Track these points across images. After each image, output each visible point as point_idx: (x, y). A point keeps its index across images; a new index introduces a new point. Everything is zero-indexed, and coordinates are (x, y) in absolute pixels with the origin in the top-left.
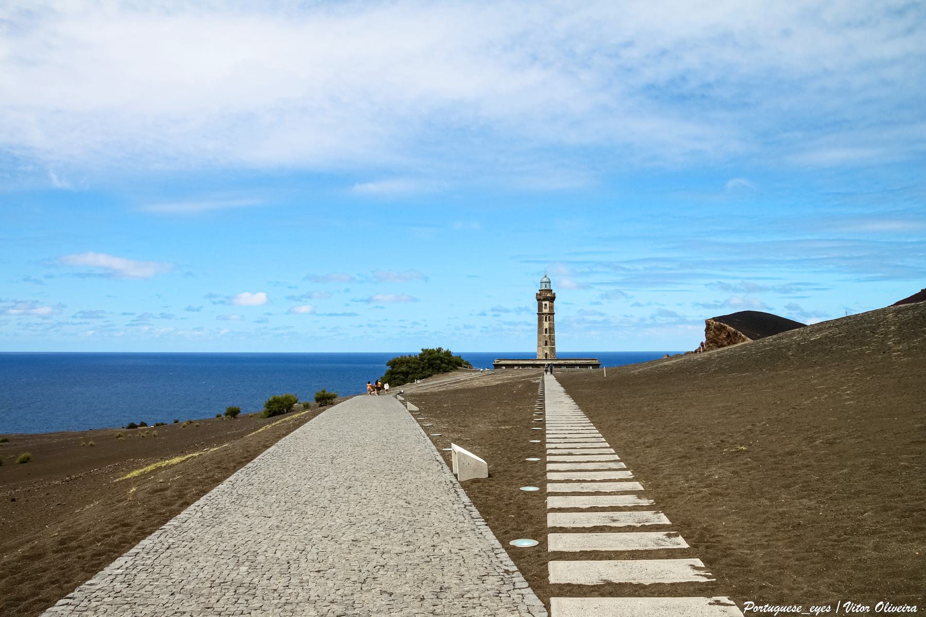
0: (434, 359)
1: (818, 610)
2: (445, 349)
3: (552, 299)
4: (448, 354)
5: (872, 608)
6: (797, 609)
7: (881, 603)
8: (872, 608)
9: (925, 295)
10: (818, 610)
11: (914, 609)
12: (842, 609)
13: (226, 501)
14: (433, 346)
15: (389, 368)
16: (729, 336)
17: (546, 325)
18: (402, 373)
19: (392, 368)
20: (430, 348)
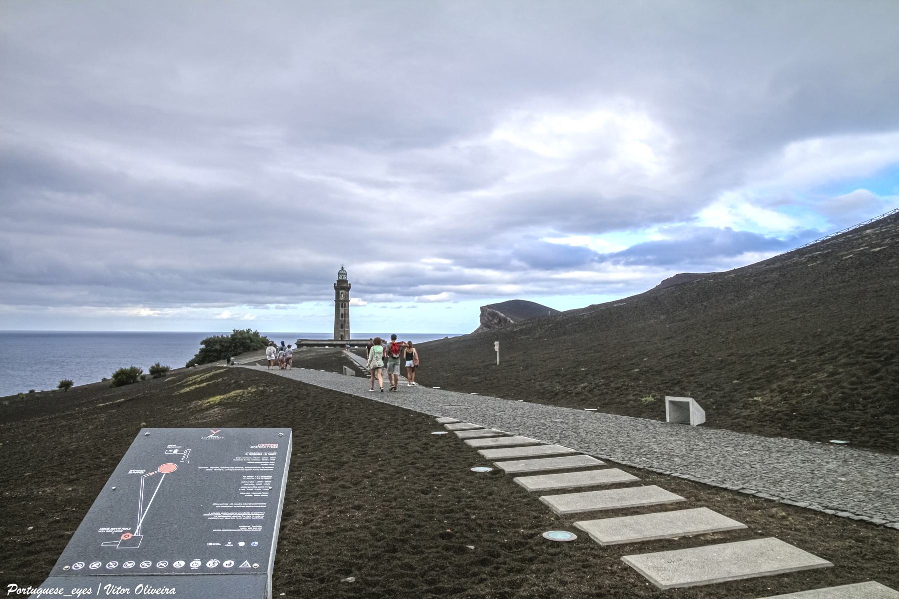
0: (244, 338)
1: (79, 592)
2: (254, 331)
3: (348, 289)
4: (256, 334)
5: (132, 591)
6: (59, 591)
7: (141, 585)
8: (132, 591)
9: (898, 218)
10: (79, 592)
11: (173, 591)
12: (103, 592)
13: (851, 589)
14: (243, 328)
15: (203, 346)
16: (500, 322)
17: (342, 311)
18: (216, 350)
19: (207, 346)
20: (241, 329)
